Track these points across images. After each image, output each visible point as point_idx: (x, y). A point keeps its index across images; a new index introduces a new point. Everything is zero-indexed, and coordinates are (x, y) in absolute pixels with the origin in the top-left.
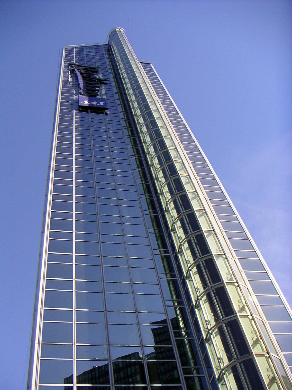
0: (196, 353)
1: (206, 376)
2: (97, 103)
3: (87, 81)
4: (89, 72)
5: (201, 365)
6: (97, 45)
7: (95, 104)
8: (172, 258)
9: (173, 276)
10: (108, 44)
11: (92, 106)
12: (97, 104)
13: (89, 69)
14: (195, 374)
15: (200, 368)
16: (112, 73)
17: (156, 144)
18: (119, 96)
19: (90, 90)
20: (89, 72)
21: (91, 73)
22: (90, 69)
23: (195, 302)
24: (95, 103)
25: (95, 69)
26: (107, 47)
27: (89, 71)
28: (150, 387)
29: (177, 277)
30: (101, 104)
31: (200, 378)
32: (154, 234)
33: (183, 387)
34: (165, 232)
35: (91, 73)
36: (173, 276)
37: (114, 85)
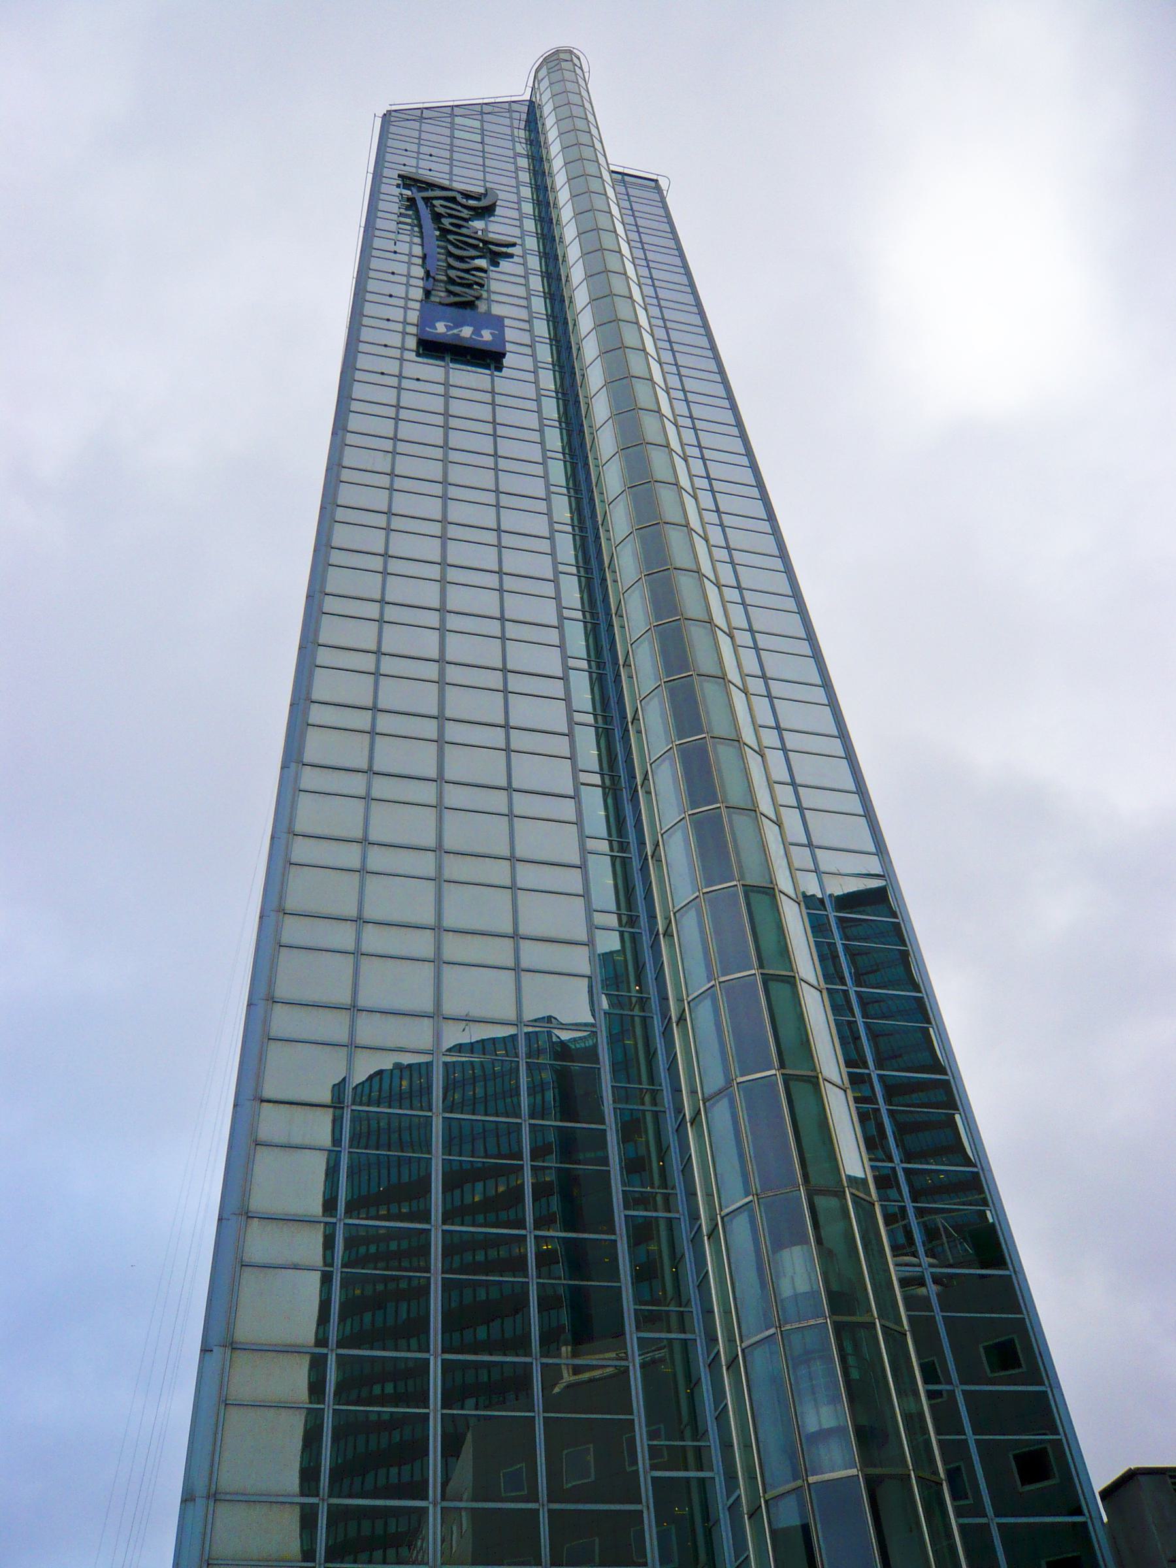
0: (615, 759)
1: (682, 1218)
2: (473, 333)
3: (451, 248)
4: (459, 211)
5: (661, 1085)
6: (493, 100)
7: (468, 336)
8: (636, 864)
9: (623, 847)
10: (529, 99)
11: (457, 342)
12: (473, 337)
13: (459, 198)
14: (637, 1012)
15: (658, 1090)
16: (528, 156)
17: (769, 1248)
18: (530, 179)
19: (459, 281)
20: (459, 211)
21: (465, 213)
22: (464, 201)
23: (694, 1111)
24: (467, 332)
25: (477, 198)
26: (525, 109)
27: (459, 208)
28: (533, 1237)
29: (632, 852)
30: (487, 335)
31: (644, 1019)
32: (558, 430)
33: (645, 1515)
34: (669, 1103)
35: (465, 213)
36: (623, 847)
37: (534, 262)
